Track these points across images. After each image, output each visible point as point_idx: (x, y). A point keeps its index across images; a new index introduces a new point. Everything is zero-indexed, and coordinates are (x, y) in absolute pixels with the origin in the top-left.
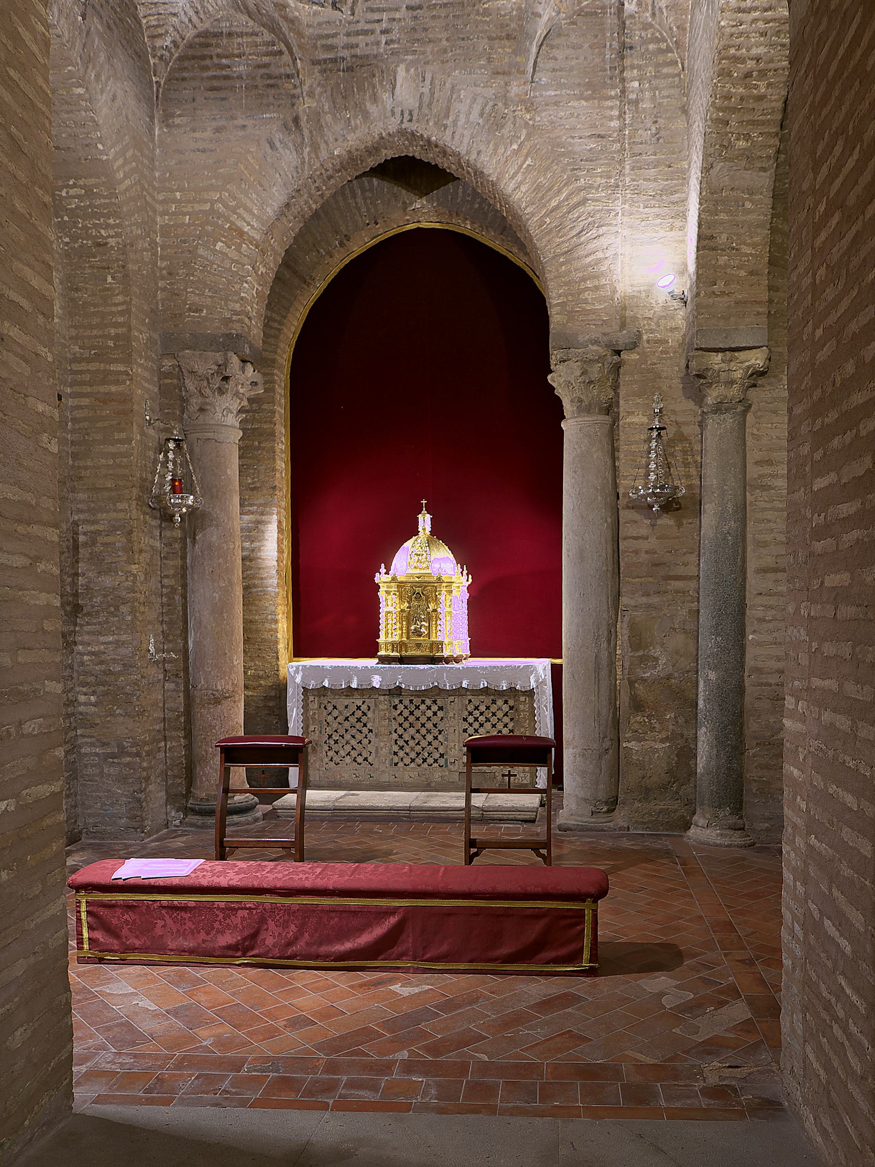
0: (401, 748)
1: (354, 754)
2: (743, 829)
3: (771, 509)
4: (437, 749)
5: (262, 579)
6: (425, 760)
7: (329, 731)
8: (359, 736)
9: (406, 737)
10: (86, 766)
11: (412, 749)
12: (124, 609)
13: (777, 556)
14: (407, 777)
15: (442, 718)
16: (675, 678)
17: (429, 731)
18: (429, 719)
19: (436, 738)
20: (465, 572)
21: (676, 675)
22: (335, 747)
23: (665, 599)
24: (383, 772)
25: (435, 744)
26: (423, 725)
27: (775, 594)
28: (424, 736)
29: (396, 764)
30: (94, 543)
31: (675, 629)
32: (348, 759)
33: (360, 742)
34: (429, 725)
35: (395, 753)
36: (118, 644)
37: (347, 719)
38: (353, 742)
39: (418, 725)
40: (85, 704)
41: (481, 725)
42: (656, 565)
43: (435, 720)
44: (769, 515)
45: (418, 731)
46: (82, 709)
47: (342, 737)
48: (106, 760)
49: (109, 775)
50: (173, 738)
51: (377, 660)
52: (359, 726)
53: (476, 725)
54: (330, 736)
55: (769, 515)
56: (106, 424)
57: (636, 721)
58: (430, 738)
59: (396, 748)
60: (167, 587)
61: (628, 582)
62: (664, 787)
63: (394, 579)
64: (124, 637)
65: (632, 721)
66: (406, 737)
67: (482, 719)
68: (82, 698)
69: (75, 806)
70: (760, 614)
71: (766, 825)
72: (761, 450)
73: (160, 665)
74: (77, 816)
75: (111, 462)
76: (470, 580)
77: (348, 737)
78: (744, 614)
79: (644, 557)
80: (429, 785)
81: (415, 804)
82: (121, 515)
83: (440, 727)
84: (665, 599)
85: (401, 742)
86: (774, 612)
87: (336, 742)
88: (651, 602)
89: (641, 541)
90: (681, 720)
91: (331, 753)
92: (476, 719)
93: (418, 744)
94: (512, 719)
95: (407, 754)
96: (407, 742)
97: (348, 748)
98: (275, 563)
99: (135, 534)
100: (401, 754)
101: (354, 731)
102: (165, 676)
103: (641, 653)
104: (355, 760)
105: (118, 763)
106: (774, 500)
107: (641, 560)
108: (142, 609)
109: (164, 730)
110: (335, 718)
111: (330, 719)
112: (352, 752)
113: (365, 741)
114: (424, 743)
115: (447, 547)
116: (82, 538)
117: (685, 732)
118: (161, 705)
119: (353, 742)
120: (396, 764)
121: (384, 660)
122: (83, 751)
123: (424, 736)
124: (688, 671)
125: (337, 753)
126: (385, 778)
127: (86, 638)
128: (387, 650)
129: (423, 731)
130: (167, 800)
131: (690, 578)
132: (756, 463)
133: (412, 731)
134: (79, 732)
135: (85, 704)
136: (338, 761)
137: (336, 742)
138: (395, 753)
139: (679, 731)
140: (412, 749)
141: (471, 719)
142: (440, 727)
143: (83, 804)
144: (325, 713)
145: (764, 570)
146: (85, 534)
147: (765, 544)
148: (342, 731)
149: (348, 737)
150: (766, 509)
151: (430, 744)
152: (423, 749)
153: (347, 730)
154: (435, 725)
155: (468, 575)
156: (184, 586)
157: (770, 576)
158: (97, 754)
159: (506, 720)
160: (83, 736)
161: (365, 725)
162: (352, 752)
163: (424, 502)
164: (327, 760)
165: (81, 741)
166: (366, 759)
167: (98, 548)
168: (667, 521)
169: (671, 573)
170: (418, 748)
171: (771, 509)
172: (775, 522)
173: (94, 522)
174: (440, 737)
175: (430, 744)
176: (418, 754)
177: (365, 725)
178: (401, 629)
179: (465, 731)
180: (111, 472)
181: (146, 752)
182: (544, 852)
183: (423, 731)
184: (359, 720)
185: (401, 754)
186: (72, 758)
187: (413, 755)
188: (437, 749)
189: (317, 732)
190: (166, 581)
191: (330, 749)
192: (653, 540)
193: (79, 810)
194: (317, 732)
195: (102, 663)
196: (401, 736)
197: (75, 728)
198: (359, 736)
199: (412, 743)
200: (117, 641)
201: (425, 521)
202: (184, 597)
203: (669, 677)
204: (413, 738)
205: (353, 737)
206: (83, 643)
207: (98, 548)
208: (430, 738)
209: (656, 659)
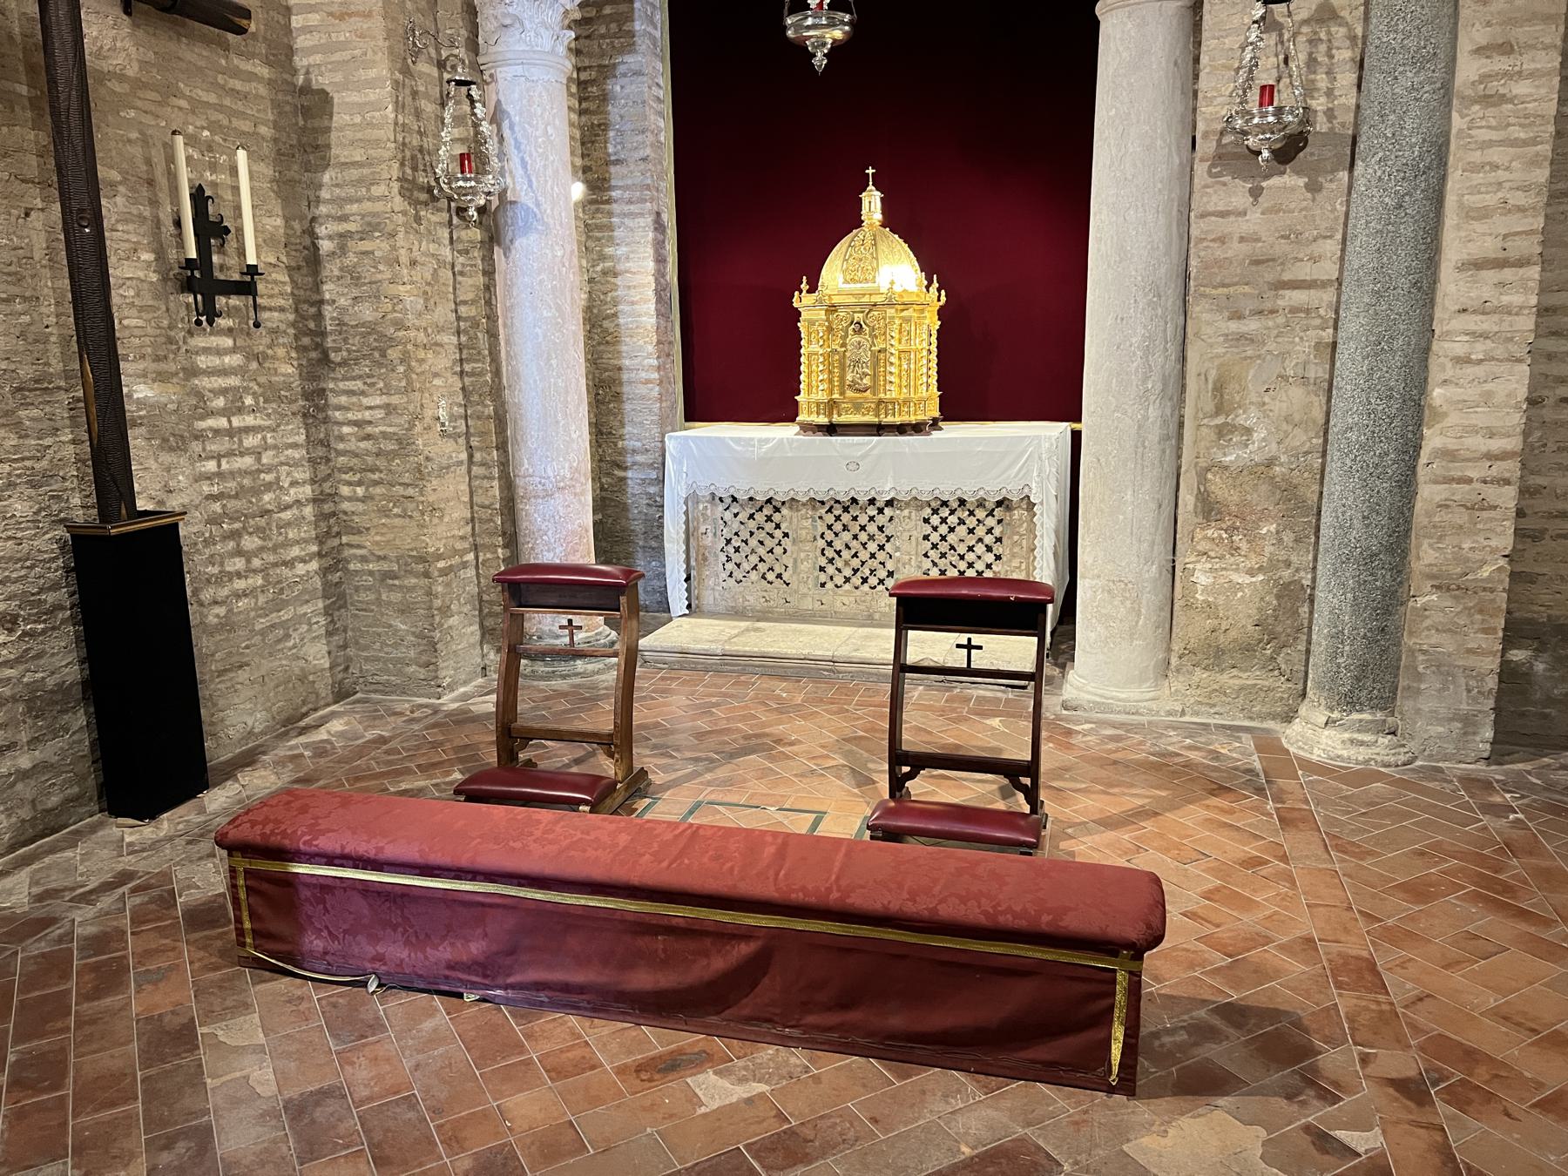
0: (831, 561)
1: (762, 567)
2: (1394, 733)
3: (1501, 143)
4: (883, 563)
5: (633, 303)
6: (865, 580)
7: (727, 533)
8: (769, 543)
9: (838, 545)
10: (357, 589)
11: (847, 563)
12: (393, 354)
13: (1505, 237)
14: (838, 604)
15: (891, 519)
16: (1281, 465)
17: (871, 537)
18: (872, 519)
19: (881, 548)
20: (936, 285)
21: (1283, 458)
22: (736, 557)
23: (1271, 324)
24: (805, 595)
25: (881, 556)
26: (863, 528)
27: (1495, 311)
28: (864, 545)
29: (823, 585)
30: (343, 250)
31: (1284, 378)
32: (754, 576)
33: (771, 551)
34: (872, 528)
35: (822, 569)
36: (389, 409)
37: (751, 517)
38: (762, 551)
39: (855, 528)
40: (350, 499)
41: (952, 530)
42: (1257, 262)
43: (881, 520)
44: (1495, 154)
45: (855, 537)
46: (346, 506)
47: (746, 542)
48: (383, 580)
49: (389, 603)
50: (486, 547)
51: (797, 428)
52: (769, 527)
53: (943, 529)
54: (728, 542)
55: (1495, 154)
56: (346, 55)
57: (1205, 538)
58: (872, 547)
59: (823, 562)
60: (465, 320)
61: (1203, 295)
62: (1248, 649)
63: (820, 301)
64: (395, 400)
65: (1199, 535)
66: (838, 545)
67: (953, 520)
68: (345, 490)
69: (345, 647)
70: (1459, 349)
71: (1441, 729)
72: (1489, 24)
73: (462, 441)
74: (349, 659)
75: (358, 119)
76: (943, 299)
77: (753, 542)
78: (1427, 350)
79: (1235, 249)
80: (870, 617)
81: (843, 652)
82: (379, 207)
83: (888, 532)
84: (1271, 324)
85: (830, 553)
86: (1489, 344)
87: (737, 550)
88: (1244, 329)
89: (1232, 218)
90: (1288, 537)
91: (730, 566)
92: (944, 521)
93: (855, 555)
94: (1000, 522)
95: (839, 570)
96: (838, 553)
97: (754, 559)
98: (652, 279)
99: (401, 235)
100: (831, 570)
101: (762, 535)
102: (471, 456)
103: (1220, 420)
104: (764, 577)
105: (400, 587)
106: (1509, 125)
107: (1230, 254)
108: (421, 354)
109: (473, 535)
110: (736, 515)
111: (728, 516)
112: (760, 565)
113: (778, 550)
114: (864, 555)
115: (906, 246)
116: (326, 246)
117: (1294, 558)
118: (466, 499)
119: (762, 551)
120: (823, 585)
121: (808, 428)
122: (352, 567)
123: (864, 545)
124: (1306, 453)
125: (738, 565)
126: (808, 604)
127: (343, 399)
128: (810, 413)
129: (863, 537)
130: (483, 636)
131: (1324, 285)
132: (1480, 51)
133: (846, 536)
134: (345, 539)
135: (350, 499)
136: (740, 577)
137: (737, 550)
138: (822, 569)
139: (1282, 555)
140: (847, 563)
141: (935, 520)
142: (888, 532)
143: (357, 643)
144: (721, 507)
145: (1478, 265)
146: (330, 238)
147: (1483, 214)
148: (745, 535)
149: (753, 542)
150: (1491, 144)
151: (873, 556)
152: (863, 563)
153: (752, 534)
154: (881, 529)
155: (939, 290)
156: (492, 318)
157: (1491, 276)
158: (371, 573)
159: (991, 522)
160: (350, 546)
161: (778, 526)
162: (760, 565)
163: (870, 171)
164: (724, 575)
165: (347, 552)
166: (779, 576)
167: (351, 259)
168: (1289, 181)
169: (1286, 277)
170: (856, 563)
171: (1501, 143)
172: (1507, 169)
173: (344, 218)
174: (888, 547)
175: (873, 556)
176: (856, 571)
177: (778, 526)
178: (831, 381)
179: (926, 538)
180: (359, 135)
181: (440, 570)
182: (1027, 781)
183: (863, 537)
184: (769, 519)
185: (831, 570)
186: (335, 577)
187: (848, 572)
188: (883, 563)
189: (710, 534)
190: (464, 310)
191: (729, 559)
192: (1255, 216)
193: (351, 652)
194: (710, 534)
195: (368, 437)
196: (830, 544)
197: (338, 534)
198: (769, 543)
199: (846, 554)
200: (388, 405)
201: (872, 203)
202: (493, 335)
203: (1270, 463)
204: (847, 547)
205: (761, 543)
206: (339, 408)
207: (351, 259)
208: (872, 547)
209: (1248, 431)
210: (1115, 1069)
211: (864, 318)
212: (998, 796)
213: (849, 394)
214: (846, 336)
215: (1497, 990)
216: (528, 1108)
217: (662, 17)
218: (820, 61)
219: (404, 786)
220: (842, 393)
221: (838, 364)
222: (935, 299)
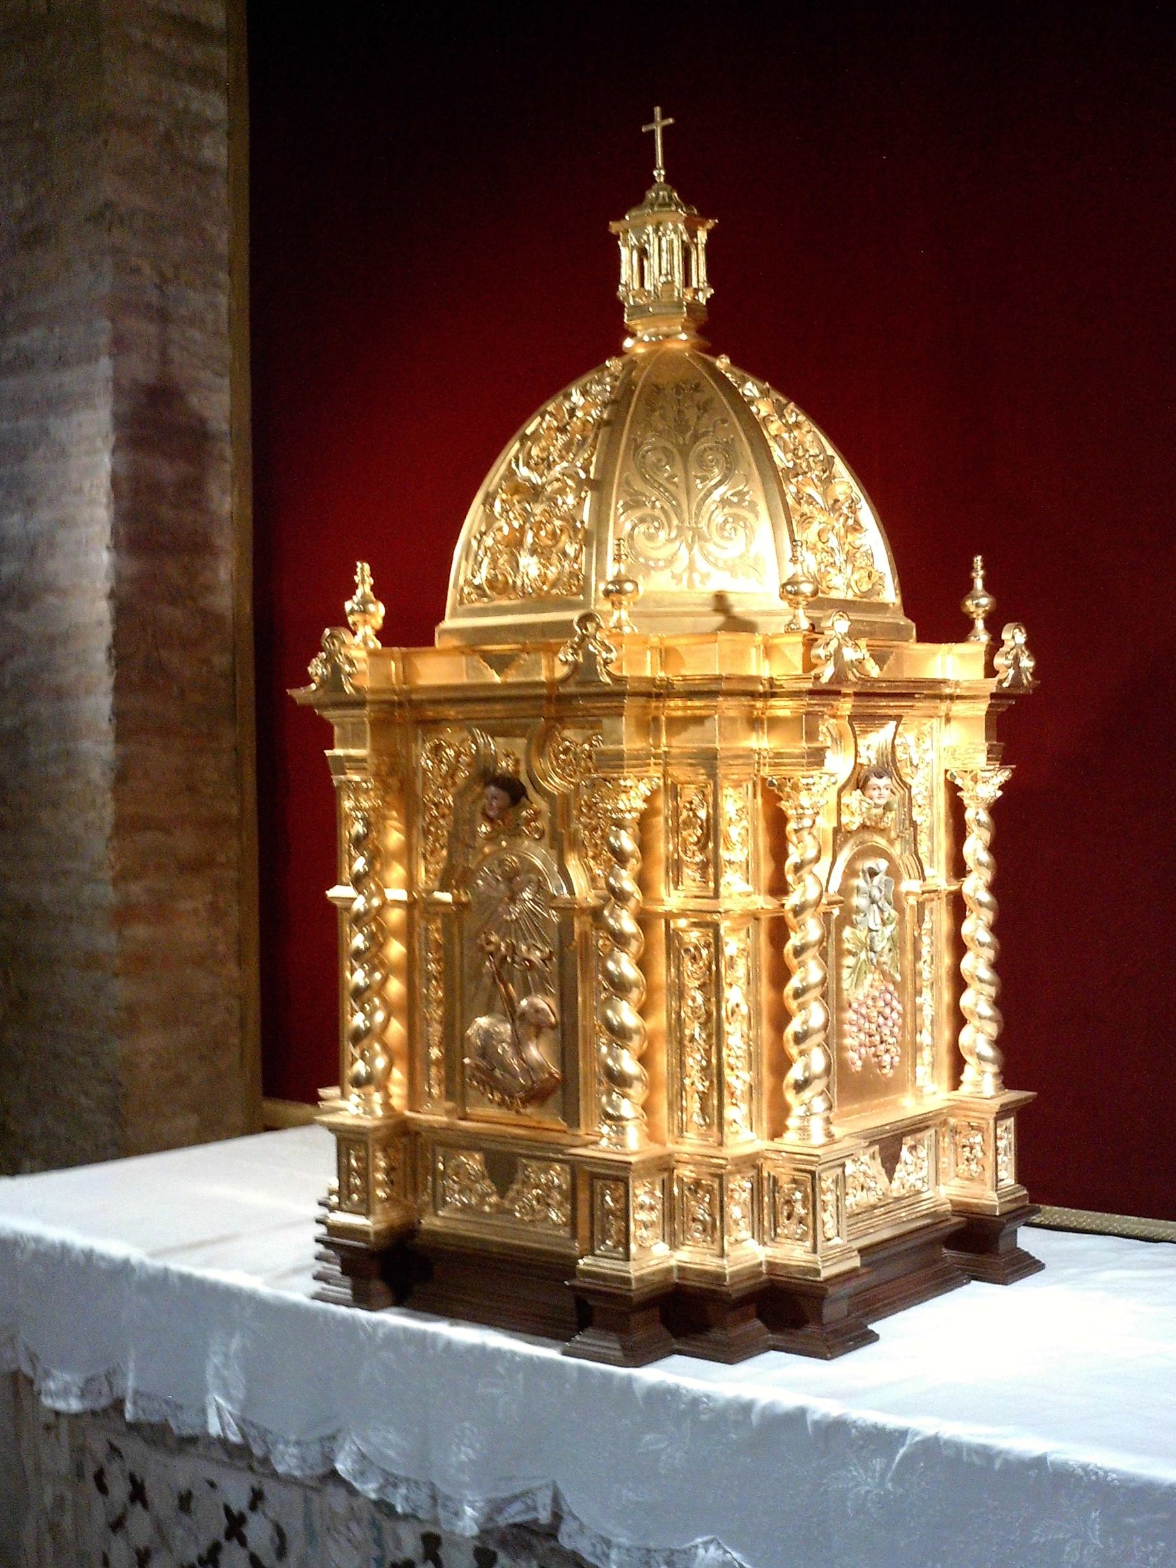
155: (994, 625)
201: (660, 259)
216: (655, 173)
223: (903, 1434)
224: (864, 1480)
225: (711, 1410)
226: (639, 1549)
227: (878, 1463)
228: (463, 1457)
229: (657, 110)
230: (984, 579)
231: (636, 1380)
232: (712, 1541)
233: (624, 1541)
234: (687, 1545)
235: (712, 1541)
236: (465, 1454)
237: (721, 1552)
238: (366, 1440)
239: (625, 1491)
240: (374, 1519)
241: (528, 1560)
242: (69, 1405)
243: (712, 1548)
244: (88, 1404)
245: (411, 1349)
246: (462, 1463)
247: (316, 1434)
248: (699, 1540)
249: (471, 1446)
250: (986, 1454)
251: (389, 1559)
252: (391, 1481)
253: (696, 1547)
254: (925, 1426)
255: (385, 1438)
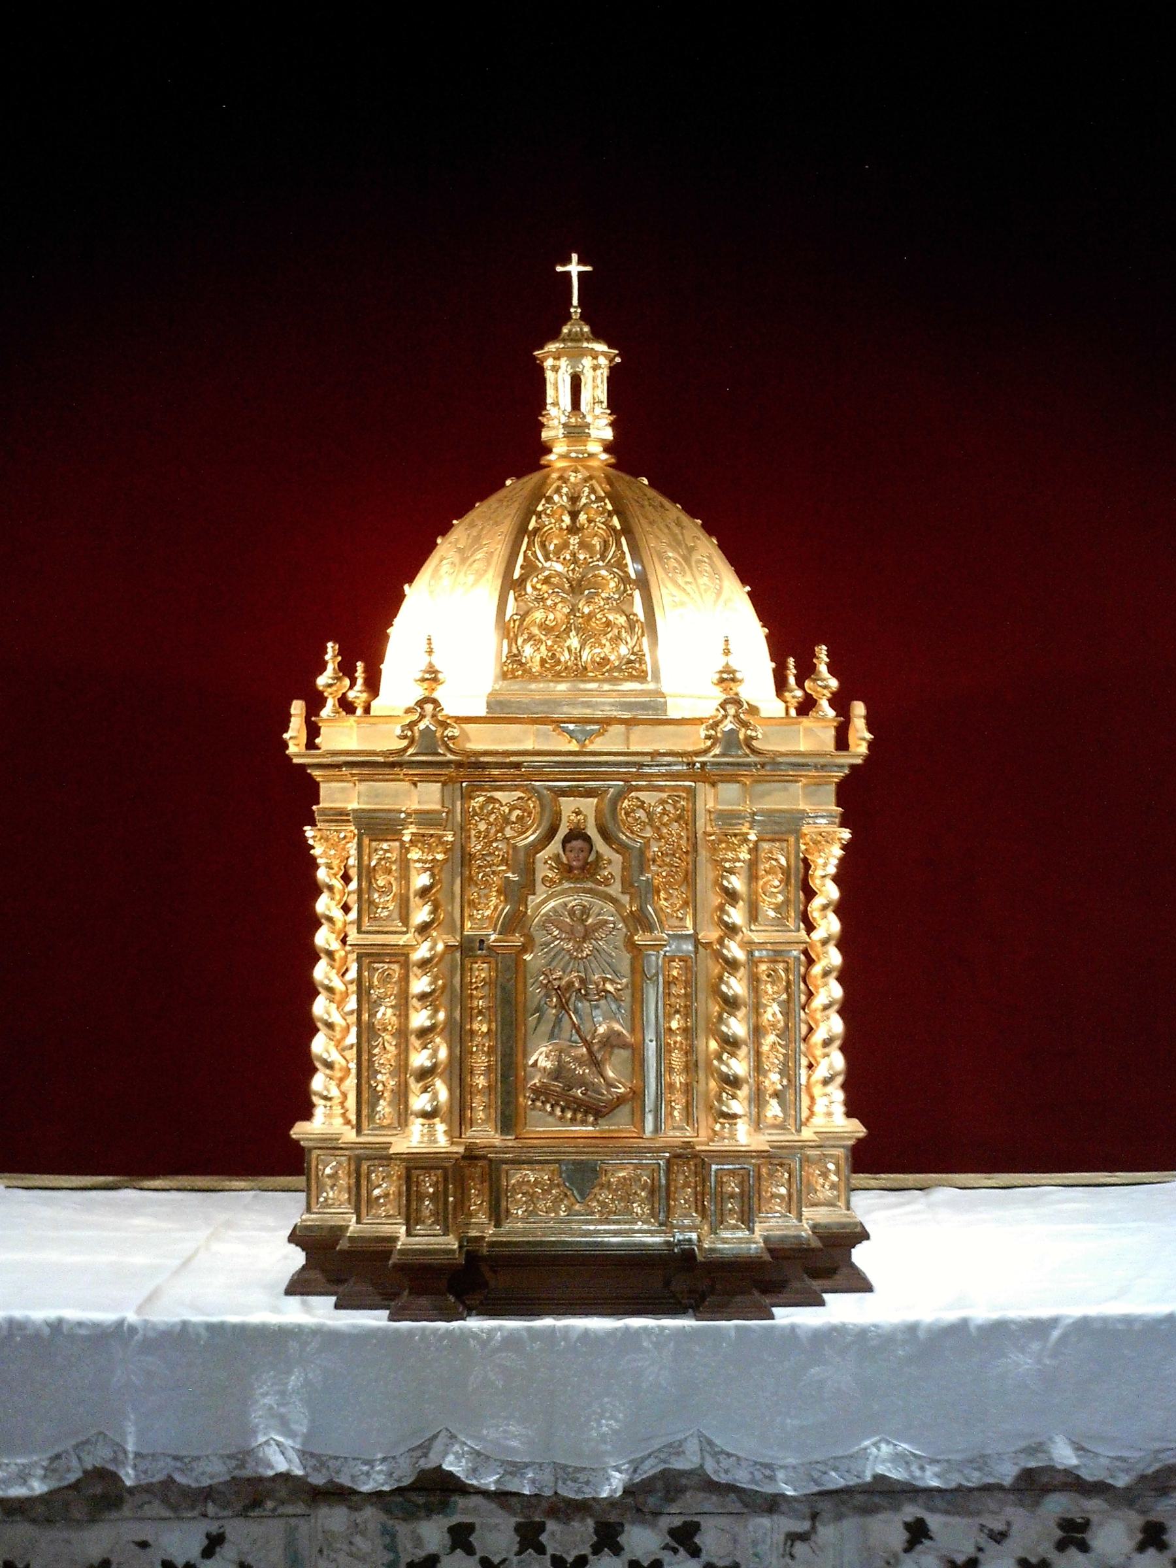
155: (840, 703)
201: (577, 384)
210: (590, 346)
211: (572, 820)
212: (1094, 1519)
213: (546, 1126)
214: (528, 885)
215: (1079, 1448)
216: (572, 310)
217: (1147, 1301)
218: (575, 257)
219: (588, 711)
220: (508, 1122)
221: (497, 995)
222: (815, 734)
223: (1054, 1322)
224: (1023, 1361)
225: (879, 1336)
226: (803, 1465)
227: (1035, 1346)
228: (605, 1429)
229: (588, 269)
230: (829, 665)
231: (799, 1326)
232: (880, 1441)
233: (791, 1461)
234: (856, 1448)
235: (880, 1441)
236: (607, 1426)
237: (891, 1447)
238: (481, 1439)
239: (789, 1421)
240: (384, 1526)
241: (583, 1520)
242: (31, 1488)
243: (883, 1446)
244: (54, 1484)
245: (537, 1345)
246: (604, 1435)
247: (403, 1449)
248: (867, 1443)
249: (613, 1417)
250: (1128, 1320)
251: (405, 1559)
252: (515, 1469)
253: (865, 1449)
254: (1074, 1311)
255: (505, 1431)
